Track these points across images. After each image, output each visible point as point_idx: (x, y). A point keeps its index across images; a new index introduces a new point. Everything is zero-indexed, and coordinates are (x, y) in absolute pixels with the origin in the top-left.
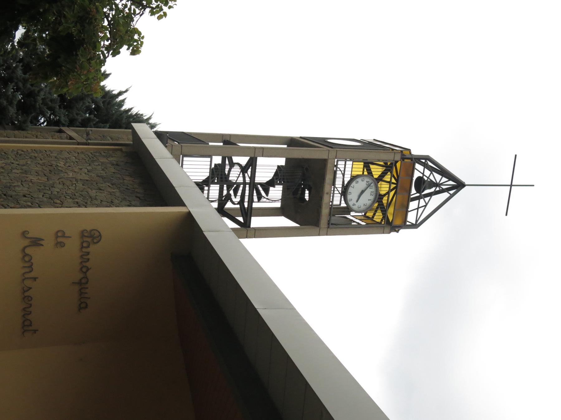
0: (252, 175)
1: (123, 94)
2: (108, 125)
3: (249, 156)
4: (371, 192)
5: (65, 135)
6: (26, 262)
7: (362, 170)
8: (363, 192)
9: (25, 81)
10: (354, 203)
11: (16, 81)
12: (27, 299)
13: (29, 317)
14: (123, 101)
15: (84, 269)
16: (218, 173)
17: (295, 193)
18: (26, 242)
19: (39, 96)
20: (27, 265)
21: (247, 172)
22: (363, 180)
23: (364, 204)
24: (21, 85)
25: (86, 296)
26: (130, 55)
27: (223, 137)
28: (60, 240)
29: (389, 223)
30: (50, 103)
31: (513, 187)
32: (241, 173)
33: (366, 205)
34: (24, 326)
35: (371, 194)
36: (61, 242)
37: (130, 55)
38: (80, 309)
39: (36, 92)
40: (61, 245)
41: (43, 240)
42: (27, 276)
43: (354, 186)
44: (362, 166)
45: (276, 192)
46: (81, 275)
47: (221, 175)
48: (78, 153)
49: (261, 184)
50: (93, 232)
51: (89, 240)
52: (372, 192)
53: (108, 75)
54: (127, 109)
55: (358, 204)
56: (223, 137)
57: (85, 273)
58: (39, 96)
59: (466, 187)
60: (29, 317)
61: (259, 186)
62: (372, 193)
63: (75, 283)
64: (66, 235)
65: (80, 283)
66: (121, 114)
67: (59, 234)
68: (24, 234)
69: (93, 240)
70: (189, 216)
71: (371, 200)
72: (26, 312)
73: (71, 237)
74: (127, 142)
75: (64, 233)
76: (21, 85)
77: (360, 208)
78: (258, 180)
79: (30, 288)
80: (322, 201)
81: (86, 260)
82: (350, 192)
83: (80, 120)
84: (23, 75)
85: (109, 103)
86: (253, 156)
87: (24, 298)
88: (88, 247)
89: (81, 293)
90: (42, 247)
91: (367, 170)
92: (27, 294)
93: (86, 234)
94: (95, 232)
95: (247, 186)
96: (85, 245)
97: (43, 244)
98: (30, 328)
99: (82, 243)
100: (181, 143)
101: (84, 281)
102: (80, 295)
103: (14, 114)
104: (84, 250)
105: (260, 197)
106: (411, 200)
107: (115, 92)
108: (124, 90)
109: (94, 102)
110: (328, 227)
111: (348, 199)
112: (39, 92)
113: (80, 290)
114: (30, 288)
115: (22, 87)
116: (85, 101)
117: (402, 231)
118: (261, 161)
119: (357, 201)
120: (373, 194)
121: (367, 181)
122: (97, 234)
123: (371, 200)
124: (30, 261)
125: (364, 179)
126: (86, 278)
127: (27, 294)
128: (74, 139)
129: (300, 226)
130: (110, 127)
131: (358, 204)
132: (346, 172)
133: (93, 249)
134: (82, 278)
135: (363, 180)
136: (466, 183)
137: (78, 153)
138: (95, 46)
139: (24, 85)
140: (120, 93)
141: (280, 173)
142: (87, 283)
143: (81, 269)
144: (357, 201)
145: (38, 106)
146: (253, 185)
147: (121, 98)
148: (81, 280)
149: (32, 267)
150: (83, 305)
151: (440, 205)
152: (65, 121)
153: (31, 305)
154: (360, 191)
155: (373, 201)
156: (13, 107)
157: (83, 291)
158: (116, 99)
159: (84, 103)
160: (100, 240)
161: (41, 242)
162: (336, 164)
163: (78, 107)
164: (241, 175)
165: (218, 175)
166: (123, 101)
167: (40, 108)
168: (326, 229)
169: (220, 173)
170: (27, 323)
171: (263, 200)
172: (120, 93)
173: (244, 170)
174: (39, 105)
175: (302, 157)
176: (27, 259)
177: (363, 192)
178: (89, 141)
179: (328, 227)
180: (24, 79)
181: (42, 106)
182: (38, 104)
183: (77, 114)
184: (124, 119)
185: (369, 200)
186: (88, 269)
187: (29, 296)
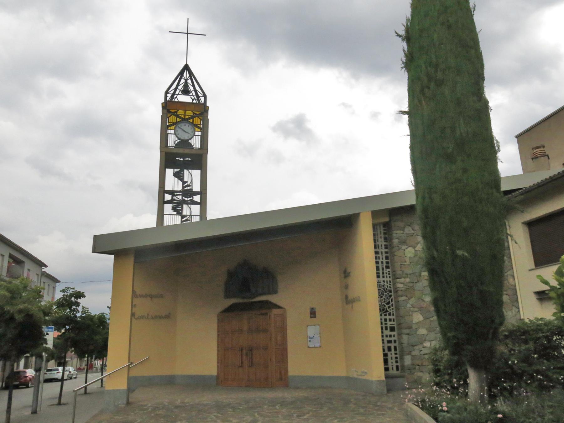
8: (184, 131)
29: (202, 114)
31: (189, 32)
38: (162, 297)
49: (183, 185)
55: (190, 133)
59: (188, 63)
61: (184, 185)
65: (151, 298)
72: (161, 317)
117: (208, 105)
118: (168, 187)
119: (189, 133)
131: (190, 133)
136: (186, 63)
138: (489, 112)
144: (189, 133)
150: (162, 296)
154: (183, 132)
162: (202, 121)
177: (184, 131)
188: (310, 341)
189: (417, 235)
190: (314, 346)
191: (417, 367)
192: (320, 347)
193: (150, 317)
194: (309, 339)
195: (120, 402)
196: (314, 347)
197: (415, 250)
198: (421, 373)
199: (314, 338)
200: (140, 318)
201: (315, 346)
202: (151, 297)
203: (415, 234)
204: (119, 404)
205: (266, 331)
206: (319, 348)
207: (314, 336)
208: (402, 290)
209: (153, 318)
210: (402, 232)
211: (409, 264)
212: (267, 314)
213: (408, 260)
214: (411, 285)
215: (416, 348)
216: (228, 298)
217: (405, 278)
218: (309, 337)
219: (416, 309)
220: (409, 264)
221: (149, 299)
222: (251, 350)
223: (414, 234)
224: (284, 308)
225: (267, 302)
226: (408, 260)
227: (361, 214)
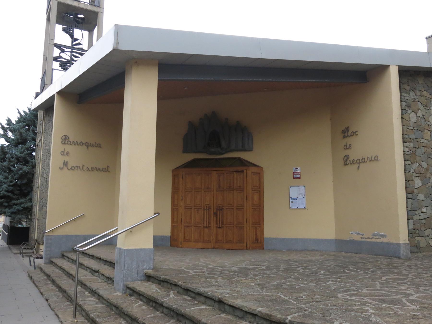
0: (65, 47)
1: (20, 112)
2: (36, 121)
3: (53, 49)
5: (39, 144)
6: (75, 169)
9: (10, 161)
11: (10, 166)
12: (92, 169)
13: (101, 169)
14: (24, 112)
15: (81, 144)
16: (64, 66)
17: (78, 22)
18: (65, 168)
19: (18, 155)
20: (76, 168)
21: (64, 50)
24: (12, 164)
25: (94, 144)
26: (36, 92)
28: (65, 153)
30: (23, 150)
34: (105, 171)
36: (67, 153)
37: (36, 92)
38: (100, 147)
39: (16, 156)
40: (68, 154)
41: (64, 161)
42: (81, 168)
45: (77, 33)
46: (84, 145)
47: (65, 64)
48: (44, 139)
49: (72, 42)
50: (63, 139)
51: (67, 141)
53: (9, 119)
54: (28, 110)
57: (83, 144)
58: (18, 155)
60: (101, 169)
63: (87, 148)
64: (63, 151)
65: (88, 146)
66: (31, 114)
67: (63, 154)
68: (61, 169)
69: (67, 139)
70: (58, 93)
72: (98, 170)
73: (64, 149)
74: (43, 113)
75: (62, 151)
76: (12, 164)
78: (70, 45)
79: (87, 167)
80: (83, 9)
81: (77, 143)
83: (33, 135)
84: (7, 162)
85: (25, 119)
86: (54, 45)
87: (92, 170)
88: (70, 141)
89: (92, 146)
90: (68, 162)
92: (90, 169)
93: (64, 142)
94: (63, 138)
95: (73, 50)
96: (69, 143)
97: (67, 161)
98: (106, 168)
99: (68, 144)
100: (44, 84)
101: (87, 144)
102: (93, 146)
103: (27, 168)
104: (72, 143)
105: (80, 44)
107: (19, 116)
108: (17, 111)
109: (24, 127)
110: (99, 7)
112: (16, 155)
113: (91, 146)
114: (87, 167)
115: (13, 163)
116: (22, 132)
118: (57, 41)
122: (64, 137)
124: (74, 167)
126: (85, 143)
127: (90, 169)
128: (40, 139)
129: (97, 26)
130: (37, 120)
133: (71, 139)
134: (85, 145)
137: (44, 139)
139: (12, 162)
140: (19, 113)
141: (66, 30)
142: (88, 143)
143: (81, 145)
145: (24, 156)
146: (72, 48)
147: (23, 114)
148: (86, 146)
149: (75, 166)
150: (99, 146)
152: (33, 143)
153: (95, 168)
156: (23, 168)
157: (91, 145)
158: (22, 115)
159: (23, 133)
160: (67, 136)
161: (66, 161)
163: (25, 136)
164: (66, 53)
165: (65, 66)
166: (24, 112)
167: (25, 155)
168: (100, 8)
169: (64, 64)
170: (104, 170)
171: (81, 43)
172: (19, 113)
173: (63, 51)
174: (23, 155)
175: (56, 16)
176: (73, 168)
178: (41, 132)
179: (99, 7)
180: (9, 162)
181: (24, 154)
182: (22, 156)
183: (30, 136)
184: (34, 112)
186: (81, 142)
187: (91, 168)
188: (292, 202)
189: (418, 101)
190: (298, 208)
191: (417, 232)
192: (305, 209)
193: (85, 168)
194: (291, 201)
195: (145, 267)
196: (298, 209)
197: (417, 115)
198: (420, 237)
199: (297, 199)
200: (73, 168)
201: (298, 208)
202: (88, 145)
203: (417, 100)
204: (144, 269)
205: (241, 189)
206: (303, 210)
207: (297, 198)
208: (407, 154)
209: (88, 169)
210: (408, 95)
211: (412, 128)
212: (242, 171)
213: (412, 125)
214: (414, 150)
215: (417, 212)
216: (185, 153)
217: (410, 142)
218: (292, 198)
219: (417, 175)
220: (412, 128)
221: (84, 147)
222: (220, 209)
223: (416, 99)
224: (262, 167)
225: (240, 159)
226: (412, 125)
227: (391, 66)
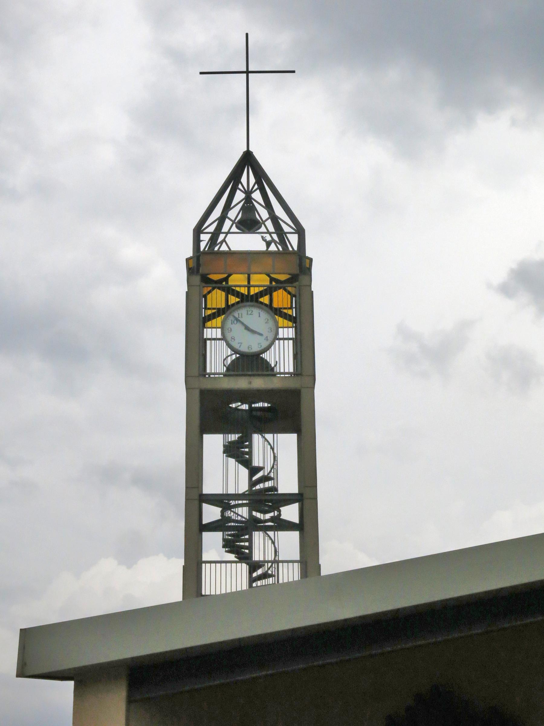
4: (247, 314)
7: (214, 306)
8: (247, 328)
10: (265, 339)
22: (230, 329)
23: (266, 323)
27: (187, 499)
29: (293, 279)
32: (233, 510)
33: (267, 320)
35: (250, 314)
43: (239, 343)
44: (219, 306)
52: (248, 312)
55: (266, 334)
56: (187, 499)
59: (250, 149)
62: (249, 313)
71: (259, 313)
77: (271, 328)
82: (248, 348)
91: (214, 314)
106: (216, 313)
111: (261, 349)
119: (261, 335)
120: (251, 312)
121: (232, 324)
123: (259, 313)
125: (228, 329)
132: (213, 307)
135: (230, 329)
136: (245, 149)
144: (261, 335)
151: (267, 175)
154: (246, 332)
155: (260, 310)
177: (247, 328)
185: (259, 316)
